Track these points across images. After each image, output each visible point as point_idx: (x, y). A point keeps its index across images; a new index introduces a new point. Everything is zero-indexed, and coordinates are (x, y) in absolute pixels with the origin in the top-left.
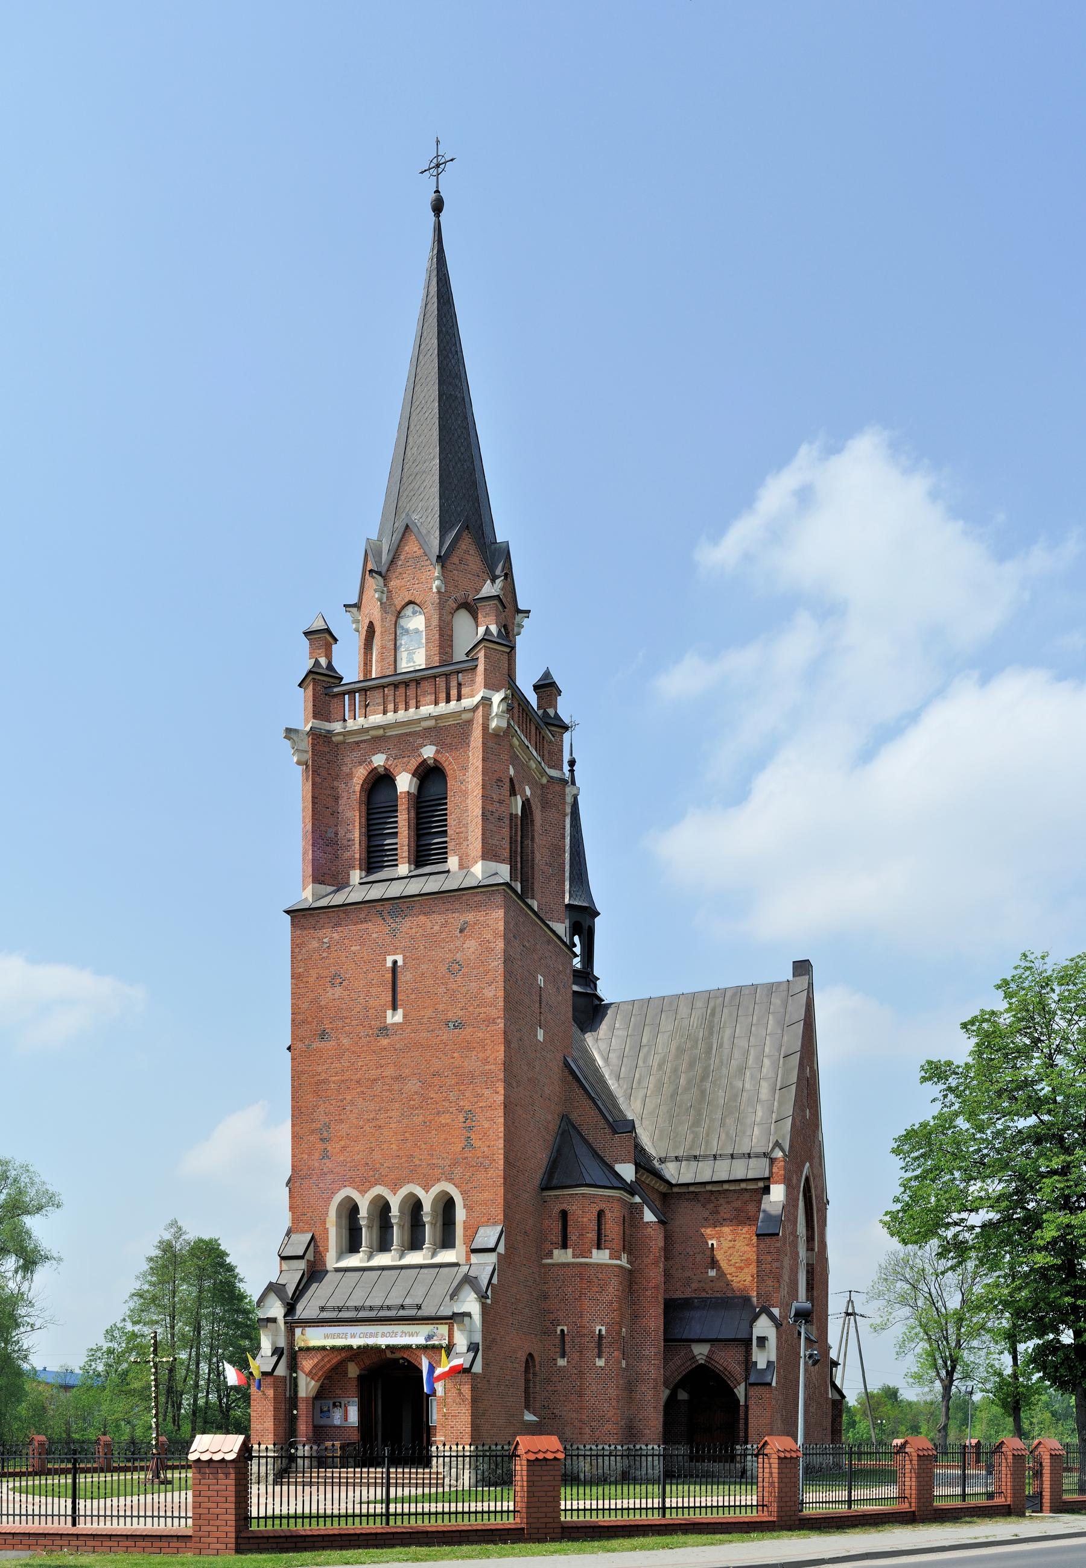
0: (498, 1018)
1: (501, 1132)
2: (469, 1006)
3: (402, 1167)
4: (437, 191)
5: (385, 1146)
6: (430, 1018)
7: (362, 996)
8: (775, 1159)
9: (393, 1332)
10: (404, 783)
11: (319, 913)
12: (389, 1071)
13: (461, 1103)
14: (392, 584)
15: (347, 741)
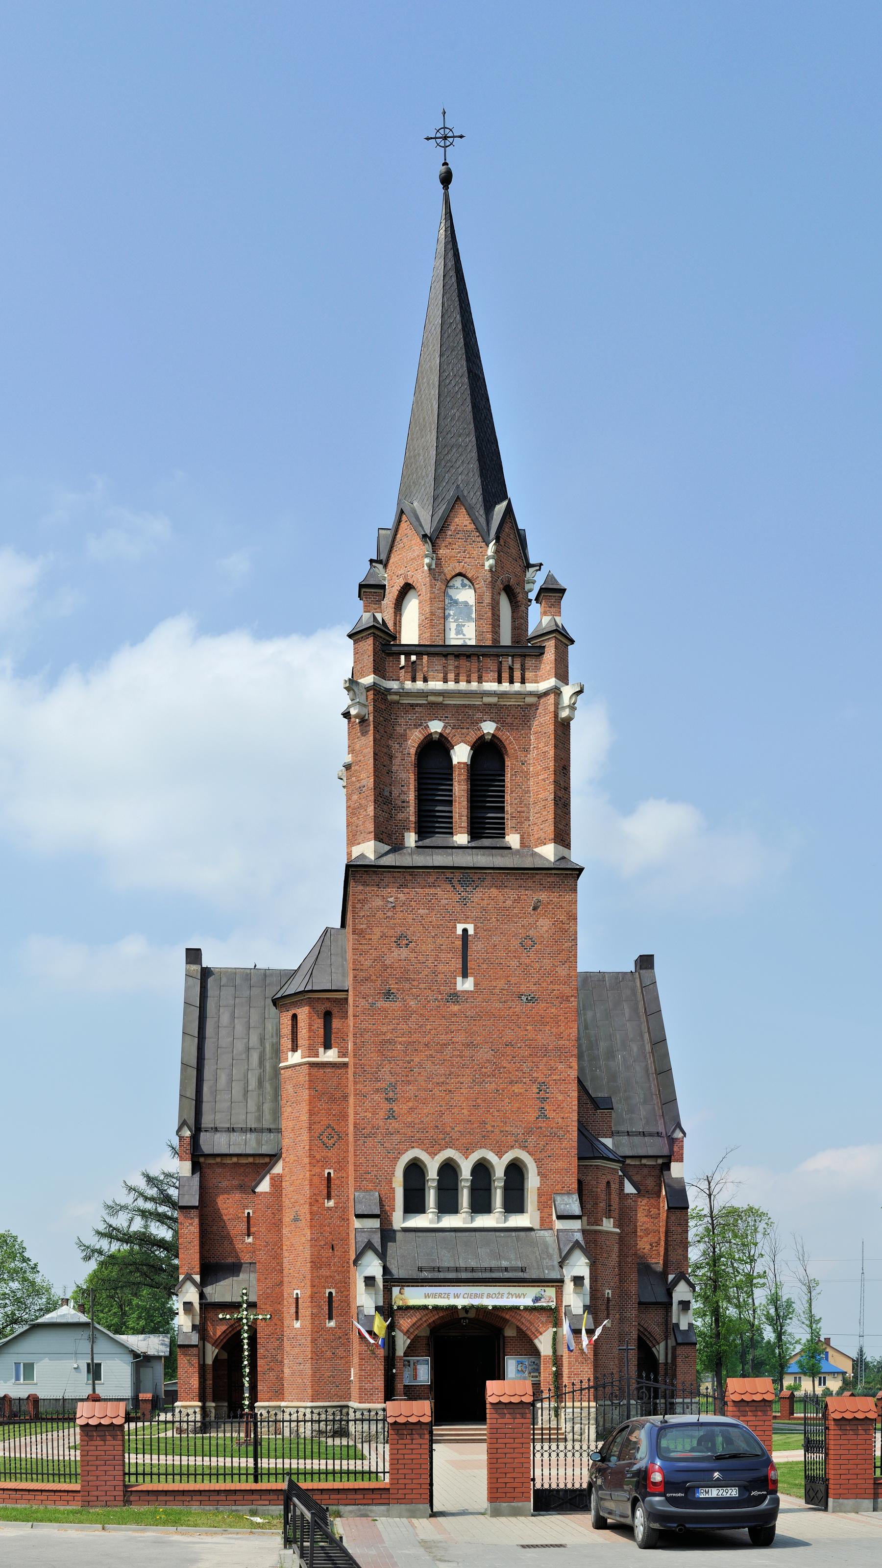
0: (572, 996)
1: (575, 1105)
2: (543, 982)
3: (473, 1132)
4: (445, 164)
5: (455, 1111)
6: (502, 989)
7: (431, 959)
8: (676, 1139)
9: (499, 1294)
10: (461, 754)
11: (383, 872)
12: (460, 1038)
13: (535, 1075)
14: (441, 552)
15: (401, 702)
